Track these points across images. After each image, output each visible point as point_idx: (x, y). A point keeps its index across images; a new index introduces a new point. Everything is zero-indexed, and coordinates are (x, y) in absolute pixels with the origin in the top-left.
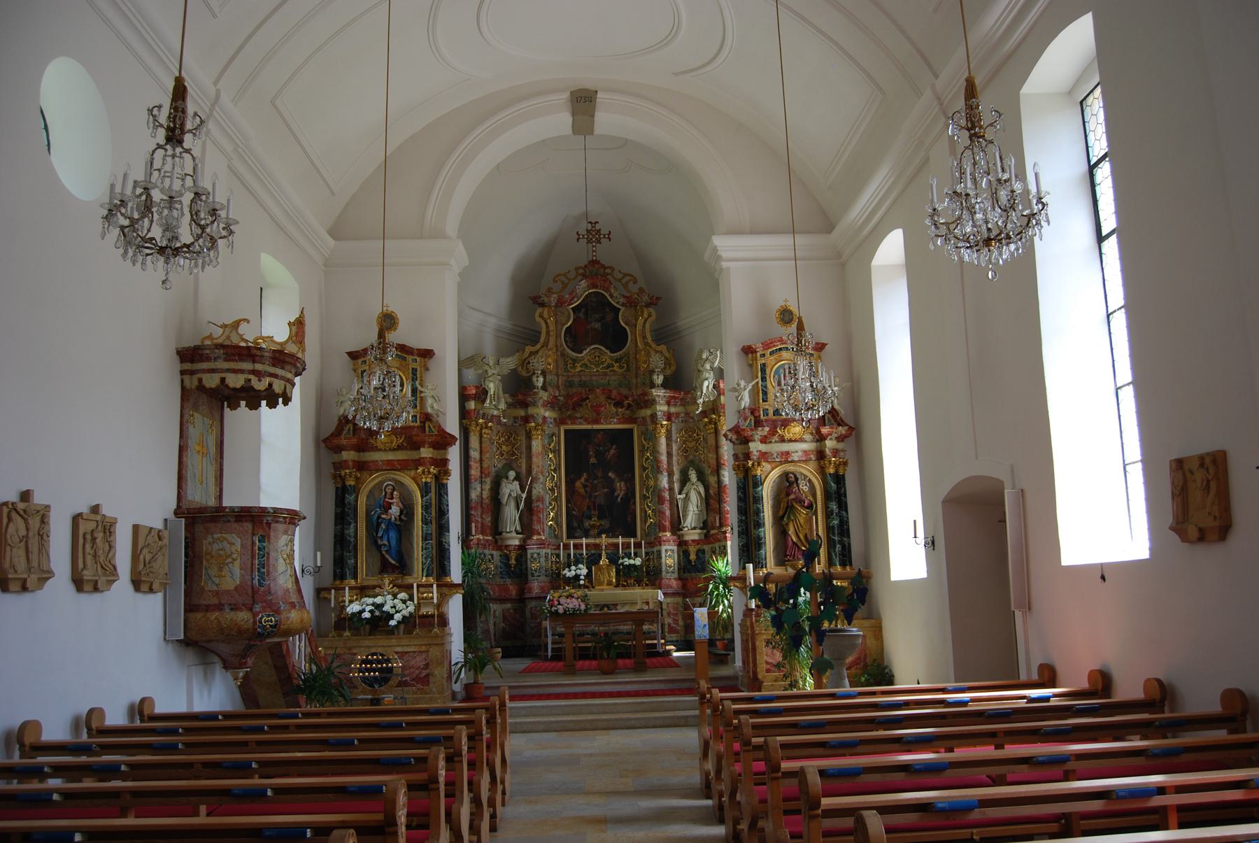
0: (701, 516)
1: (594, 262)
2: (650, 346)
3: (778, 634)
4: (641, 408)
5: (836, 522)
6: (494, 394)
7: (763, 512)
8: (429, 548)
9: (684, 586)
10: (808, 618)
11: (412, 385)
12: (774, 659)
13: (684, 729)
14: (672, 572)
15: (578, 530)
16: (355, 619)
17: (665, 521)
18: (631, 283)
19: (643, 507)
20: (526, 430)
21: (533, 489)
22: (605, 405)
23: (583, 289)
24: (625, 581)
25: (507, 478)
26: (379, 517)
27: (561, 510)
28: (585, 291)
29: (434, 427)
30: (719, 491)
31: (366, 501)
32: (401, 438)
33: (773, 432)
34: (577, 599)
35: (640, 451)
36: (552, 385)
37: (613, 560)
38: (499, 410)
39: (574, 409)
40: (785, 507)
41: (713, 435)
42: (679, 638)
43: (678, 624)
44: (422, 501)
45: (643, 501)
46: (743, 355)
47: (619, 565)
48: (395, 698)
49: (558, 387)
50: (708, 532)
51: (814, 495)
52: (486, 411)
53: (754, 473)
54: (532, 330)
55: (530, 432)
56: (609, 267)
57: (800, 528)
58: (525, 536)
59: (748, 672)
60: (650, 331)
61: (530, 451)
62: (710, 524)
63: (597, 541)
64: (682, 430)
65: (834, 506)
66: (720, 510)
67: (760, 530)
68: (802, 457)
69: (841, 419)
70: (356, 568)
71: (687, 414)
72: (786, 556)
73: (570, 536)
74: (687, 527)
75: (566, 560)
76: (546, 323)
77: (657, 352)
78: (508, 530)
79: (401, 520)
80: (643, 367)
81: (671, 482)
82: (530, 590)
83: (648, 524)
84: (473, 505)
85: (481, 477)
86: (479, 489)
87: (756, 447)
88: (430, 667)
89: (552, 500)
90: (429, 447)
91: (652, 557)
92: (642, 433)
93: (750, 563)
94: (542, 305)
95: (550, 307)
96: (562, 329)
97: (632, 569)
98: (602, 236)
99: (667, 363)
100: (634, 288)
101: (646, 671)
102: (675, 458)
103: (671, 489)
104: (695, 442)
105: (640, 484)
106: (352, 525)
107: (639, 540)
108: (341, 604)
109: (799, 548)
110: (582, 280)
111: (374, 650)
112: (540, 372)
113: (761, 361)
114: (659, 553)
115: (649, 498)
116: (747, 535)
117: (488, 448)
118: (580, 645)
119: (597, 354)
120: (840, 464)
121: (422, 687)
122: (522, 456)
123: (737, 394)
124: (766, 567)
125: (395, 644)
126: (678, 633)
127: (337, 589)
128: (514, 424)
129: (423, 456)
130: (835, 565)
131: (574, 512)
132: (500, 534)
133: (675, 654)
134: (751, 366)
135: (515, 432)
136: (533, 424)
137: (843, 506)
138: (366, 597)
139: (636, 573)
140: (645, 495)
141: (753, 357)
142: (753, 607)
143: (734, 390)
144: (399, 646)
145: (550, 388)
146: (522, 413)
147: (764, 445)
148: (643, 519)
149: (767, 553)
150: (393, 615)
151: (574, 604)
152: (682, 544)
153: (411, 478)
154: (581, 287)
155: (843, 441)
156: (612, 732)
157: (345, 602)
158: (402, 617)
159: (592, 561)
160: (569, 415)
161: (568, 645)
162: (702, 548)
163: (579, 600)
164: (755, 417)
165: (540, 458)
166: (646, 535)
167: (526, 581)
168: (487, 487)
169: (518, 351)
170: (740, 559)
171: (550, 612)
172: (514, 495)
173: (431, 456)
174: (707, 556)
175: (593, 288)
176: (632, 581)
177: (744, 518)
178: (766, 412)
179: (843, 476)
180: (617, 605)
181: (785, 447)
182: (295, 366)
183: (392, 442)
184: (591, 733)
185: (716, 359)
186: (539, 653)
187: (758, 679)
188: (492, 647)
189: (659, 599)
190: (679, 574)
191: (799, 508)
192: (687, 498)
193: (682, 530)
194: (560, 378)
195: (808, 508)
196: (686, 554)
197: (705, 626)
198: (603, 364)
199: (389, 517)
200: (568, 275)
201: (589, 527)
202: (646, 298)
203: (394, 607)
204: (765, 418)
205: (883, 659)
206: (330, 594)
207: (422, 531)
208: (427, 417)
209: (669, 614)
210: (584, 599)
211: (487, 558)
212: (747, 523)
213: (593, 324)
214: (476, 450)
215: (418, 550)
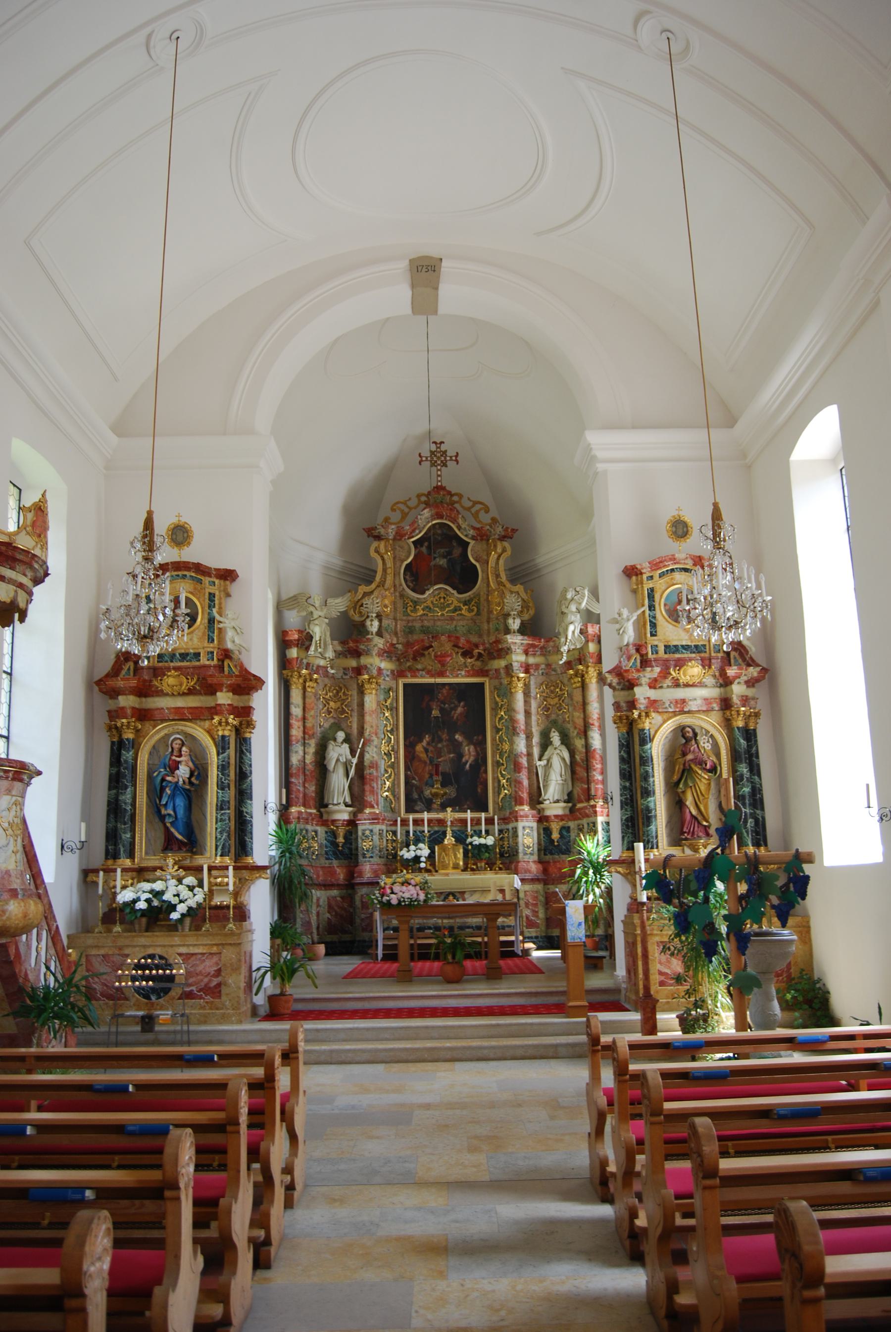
0: (565, 786)
1: (439, 489)
2: (504, 586)
3: (677, 935)
4: (494, 658)
5: (747, 790)
6: (320, 640)
7: (653, 776)
8: (225, 820)
9: (545, 871)
10: (725, 918)
11: (209, 614)
12: (669, 968)
13: (553, 1062)
16: (128, 910)
17: (523, 793)
18: (483, 511)
19: (496, 775)
20: (358, 684)
21: (366, 754)
22: (451, 655)
23: (425, 519)
24: (474, 864)
25: (335, 740)
26: (163, 780)
27: (399, 779)
28: (428, 522)
29: (235, 666)
31: (148, 760)
32: (192, 679)
33: (665, 674)
34: (415, 886)
35: (492, 709)
36: (389, 630)
37: (460, 839)
38: (325, 658)
39: (415, 659)
40: (681, 771)
41: (579, 691)
42: (538, 934)
43: (537, 917)
44: (218, 759)
45: (496, 768)
46: (624, 578)
47: (467, 845)
48: (174, 1016)
49: (396, 634)
50: (574, 805)
51: (718, 755)
52: (311, 660)
53: (640, 726)
55: (363, 686)
56: (456, 494)
57: (701, 798)
58: (355, 809)
59: (636, 984)
60: (505, 570)
61: (363, 709)
62: (576, 796)
63: (441, 816)
64: (542, 684)
65: (744, 769)
66: (588, 780)
67: (649, 799)
68: (701, 706)
69: (751, 658)
70: (132, 844)
71: (548, 665)
72: (683, 833)
73: (409, 809)
75: (404, 838)
76: (383, 559)
77: (512, 592)
78: (335, 802)
79: (191, 783)
80: (496, 610)
81: (529, 746)
82: (361, 874)
83: (502, 796)
84: (294, 772)
85: (304, 739)
86: (301, 753)
87: (642, 693)
88: (223, 974)
89: (389, 766)
90: (228, 691)
91: (506, 835)
92: (495, 688)
93: (639, 842)
94: (378, 538)
95: (388, 540)
96: (401, 566)
97: (483, 850)
98: (448, 458)
99: (525, 606)
100: (485, 518)
101: (501, 978)
102: (534, 718)
103: (529, 755)
104: (557, 698)
105: (492, 749)
106: (129, 790)
107: (491, 815)
108: (113, 890)
109: (699, 823)
110: (424, 509)
111: (150, 951)
112: (374, 615)
113: (648, 585)
114: (515, 830)
115: (503, 764)
116: (632, 807)
118: (419, 942)
119: (442, 595)
120: (750, 716)
121: (212, 999)
122: (353, 714)
123: (617, 626)
124: (657, 848)
125: (178, 943)
126: (538, 927)
127: (105, 871)
128: (346, 677)
129: (220, 702)
130: (747, 845)
131: (414, 781)
132: (326, 806)
133: (536, 954)
134: (635, 592)
135: (345, 686)
136: (366, 677)
137: (755, 769)
138: (144, 881)
139: (487, 855)
140: (498, 762)
141: (637, 580)
142: (645, 899)
143: (615, 621)
144: (184, 945)
146: (353, 663)
147: (653, 691)
148: (497, 789)
149: (659, 829)
150: (175, 905)
151: (412, 893)
152: (542, 819)
153: (205, 730)
154: (423, 517)
155: (753, 686)
156: (458, 1065)
157: (115, 887)
158: (187, 909)
159: (436, 840)
160: (409, 667)
161: (404, 943)
162: (567, 825)
163: (418, 888)
164: (642, 656)
165: (374, 716)
166: (500, 809)
167: (357, 864)
168: (311, 750)
169: (349, 592)
170: (623, 837)
171: (380, 902)
172: (343, 759)
173: (229, 702)
174: (573, 835)
175: (438, 518)
176: (483, 864)
177: (628, 784)
178: (655, 649)
179: (755, 730)
180: (464, 893)
181: (680, 693)
182: (31, 567)
183: (181, 685)
184: (429, 1066)
185: (583, 599)
186: (369, 951)
187: (651, 996)
188: (313, 943)
189: (516, 886)
190: (539, 855)
191: (700, 772)
192: (548, 765)
193: (543, 803)
194: (399, 622)
195: (710, 771)
196: (547, 831)
197: (580, 924)
198: (449, 607)
199: (176, 780)
200: (408, 503)
201: (430, 796)
202: (499, 530)
203: (178, 895)
204: (655, 656)
205: (812, 969)
206: (98, 877)
207: (218, 798)
208: (226, 654)
209: (527, 905)
210: (424, 886)
211: (309, 835)
212: (631, 791)
213: (438, 560)
215: (211, 822)
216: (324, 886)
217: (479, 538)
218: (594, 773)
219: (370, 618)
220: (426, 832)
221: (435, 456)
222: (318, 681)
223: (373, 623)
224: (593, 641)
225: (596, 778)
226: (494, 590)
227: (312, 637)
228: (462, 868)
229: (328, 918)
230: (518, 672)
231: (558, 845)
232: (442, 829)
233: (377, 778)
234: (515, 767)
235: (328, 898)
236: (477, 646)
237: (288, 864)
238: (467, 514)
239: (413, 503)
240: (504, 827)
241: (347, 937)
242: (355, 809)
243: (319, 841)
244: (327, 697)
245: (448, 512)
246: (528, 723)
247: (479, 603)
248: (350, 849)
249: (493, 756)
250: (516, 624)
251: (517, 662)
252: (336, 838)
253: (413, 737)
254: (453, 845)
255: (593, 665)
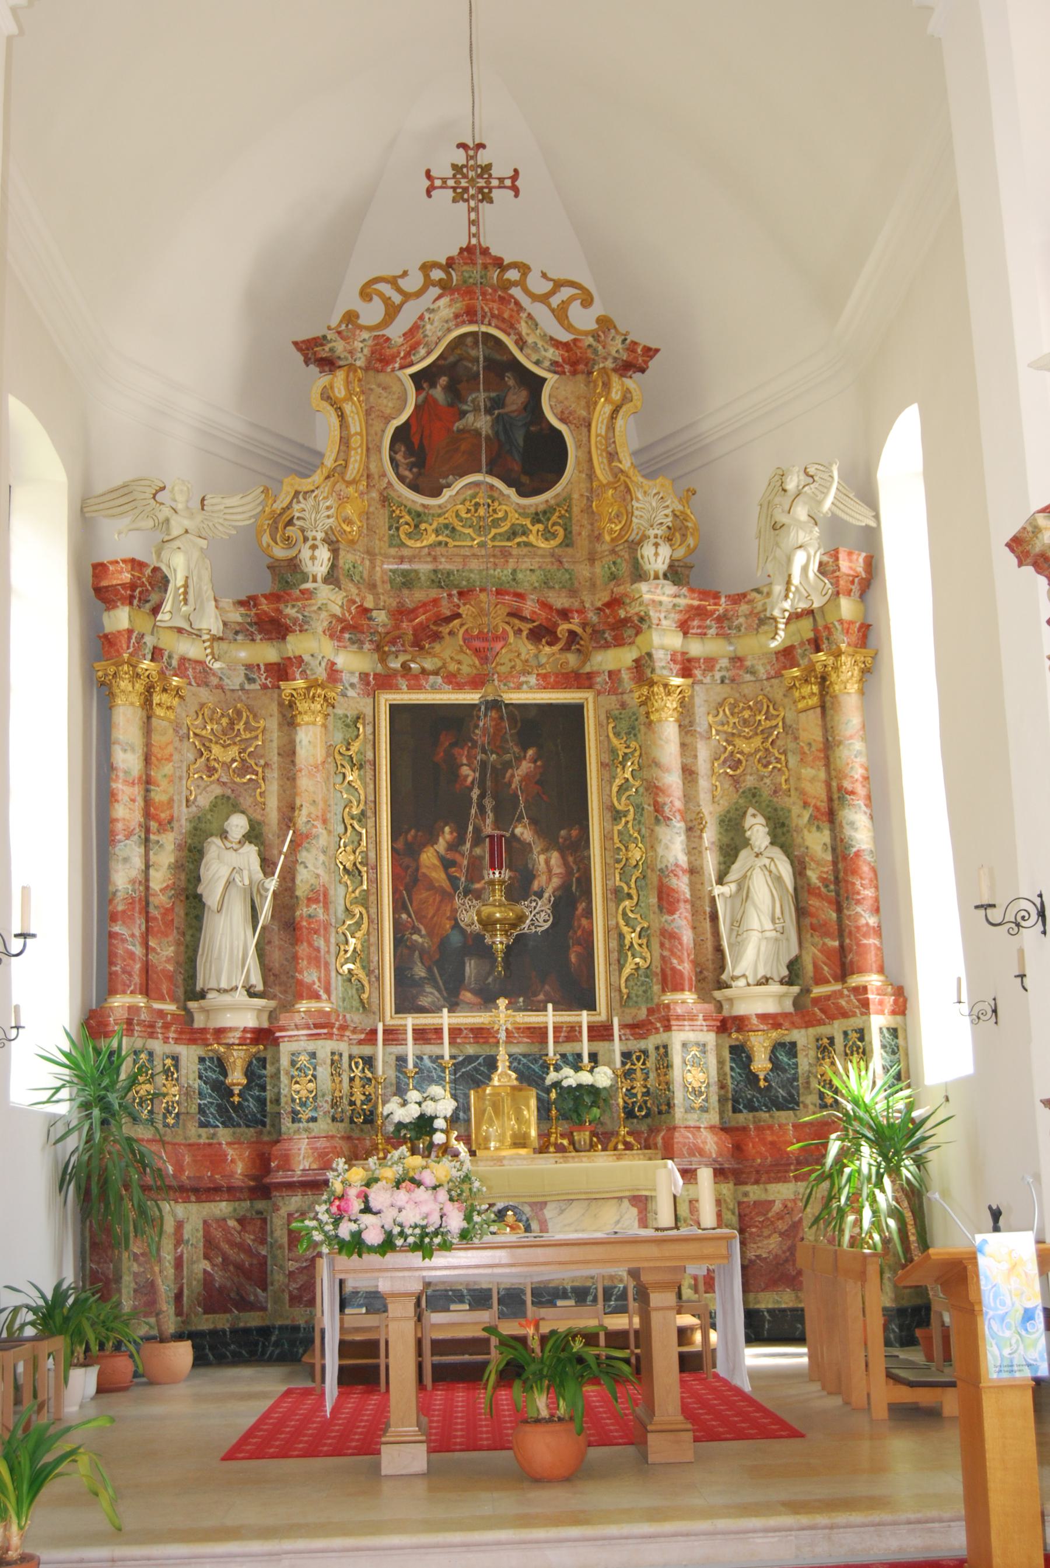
4: (607, 646)
6: (186, 586)
14: (704, 1110)
15: (429, 989)
17: (681, 962)
19: (613, 923)
21: (300, 868)
22: (504, 637)
24: (562, 1136)
25: (224, 835)
27: (379, 931)
28: (449, 330)
30: (836, 871)
35: (603, 765)
36: (356, 578)
39: (417, 644)
41: (814, 716)
45: (612, 905)
47: (548, 1091)
50: (806, 991)
54: (302, 446)
55: (292, 705)
56: (514, 265)
58: (272, 1004)
73: (405, 1004)
74: (744, 976)
78: (224, 985)
81: (693, 850)
83: (627, 971)
86: (138, 862)
89: (356, 901)
95: (352, 368)
97: (587, 1100)
98: (495, 183)
103: (694, 871)
105: (604, 857)
112: (320, 535)
114: (664, 1051)
117: (170, 749)
122: (268, 775)
128: (252, 687)
131: (415, 937)
135: (250, 709)
145: (351, 585)
146: (269, 653)
151: (425, 1209)
162: (787, 1039)
163: (442, 1195)
168: (165, 856)
174: (804, 1062)
185: (826, 494)
190: (721, 1113)
193: (728, 987)
196: (740, 1054)
201: (477, 927)
213: (470, 417)
214: (133, 750)
216: (196, 1191)
217: (567, 368)
218: (859, 909)
219: (310, 543)
220: (447, 1057)
221: (465, 176)
222: (182, 693)
223: (317, 553)
224: (849, 593)
225: (863, 921)
226: (604, 487)
227: (165, 581)
228: (536, 1145)
229: (205, 1271)
230: (665, 672)
231: (769, 1088)
232: (484, 1051)
233: (327, 926)
234: (660, 899)
235: (205, 1222)
236: (565, 614)
237: (97, 1136)
238: (540, 312)
239: (413, 282)
240: (634, 1045)
241: (252, 1320)
242: (272, 1004)
243: (183, 1080)
244: (204, 733)
245: (495, 306)
246: (689, 797)
247: (570, 518)
248: (262, 1102)
249: (606, 877)
250: (660, 560)
251: (663, 648)
252: (226, 1075)
253: (413, 832)
254: (513, 1088)
255: (851, 650)
